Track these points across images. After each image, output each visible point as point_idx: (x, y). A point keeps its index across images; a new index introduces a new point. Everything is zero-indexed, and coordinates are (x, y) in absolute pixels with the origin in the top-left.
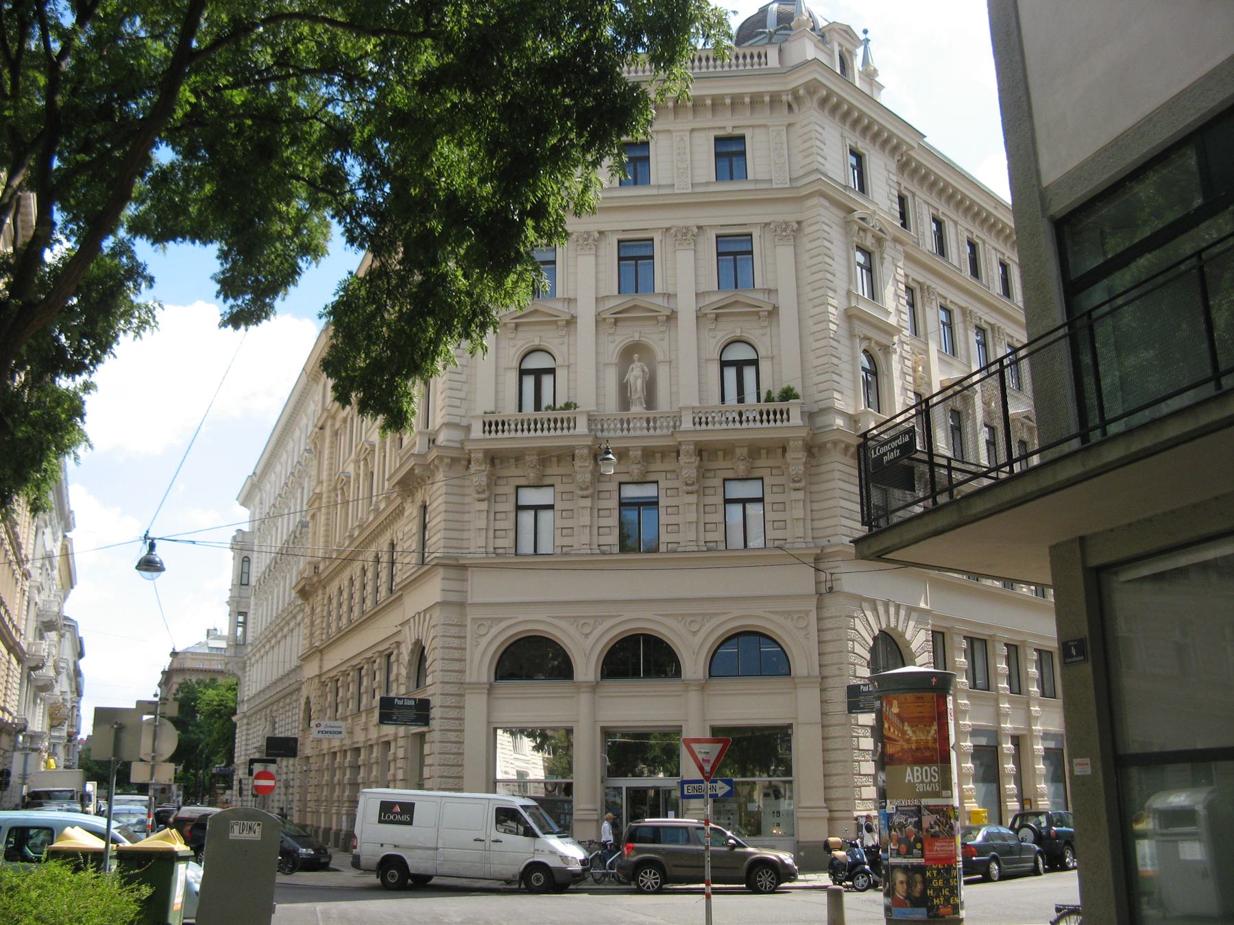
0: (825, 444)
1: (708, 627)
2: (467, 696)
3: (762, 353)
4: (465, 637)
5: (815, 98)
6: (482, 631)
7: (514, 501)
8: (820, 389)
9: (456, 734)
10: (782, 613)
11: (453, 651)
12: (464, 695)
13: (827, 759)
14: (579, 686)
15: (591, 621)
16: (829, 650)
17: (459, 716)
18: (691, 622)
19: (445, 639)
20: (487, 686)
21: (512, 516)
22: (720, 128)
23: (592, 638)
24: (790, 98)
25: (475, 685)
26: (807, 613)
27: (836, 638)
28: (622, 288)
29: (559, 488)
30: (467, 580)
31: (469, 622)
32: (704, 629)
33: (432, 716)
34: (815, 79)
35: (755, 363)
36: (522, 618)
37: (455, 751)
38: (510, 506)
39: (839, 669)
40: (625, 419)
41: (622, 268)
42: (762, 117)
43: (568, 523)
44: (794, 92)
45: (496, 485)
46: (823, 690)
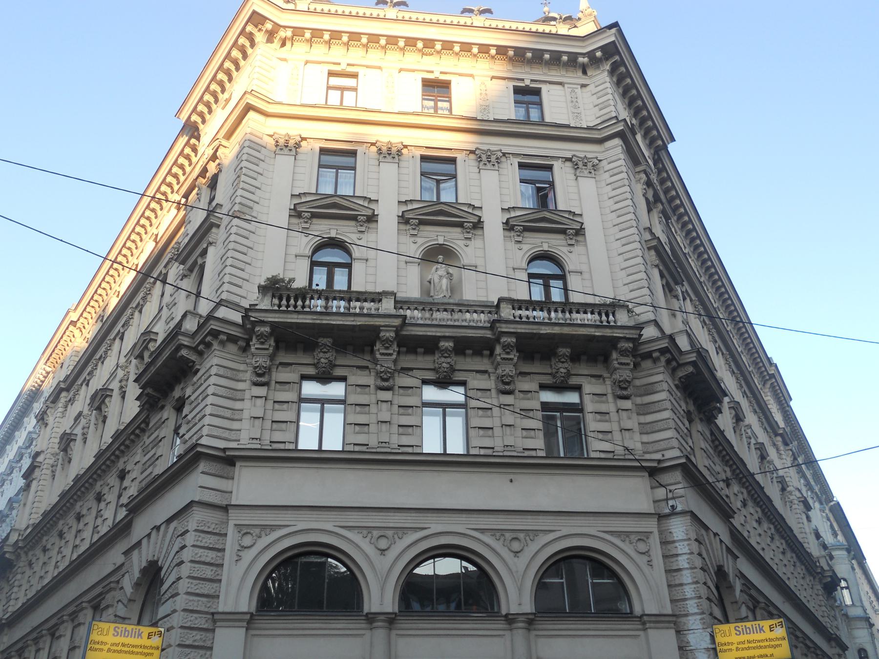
0: (651, 353)
1: (534, 547)
3: (570, 266)
4: (223, 550)
6: (247, 541)
10: (492, 531)
12: (213, 631)
19: (197, 550)
20: (248, 617)
22: (334, 64)
23: (392, 554)
25: (231, 618)
31: (231, 531)
36: (565, 531)
43: (362, 419)
46: (678, 632)
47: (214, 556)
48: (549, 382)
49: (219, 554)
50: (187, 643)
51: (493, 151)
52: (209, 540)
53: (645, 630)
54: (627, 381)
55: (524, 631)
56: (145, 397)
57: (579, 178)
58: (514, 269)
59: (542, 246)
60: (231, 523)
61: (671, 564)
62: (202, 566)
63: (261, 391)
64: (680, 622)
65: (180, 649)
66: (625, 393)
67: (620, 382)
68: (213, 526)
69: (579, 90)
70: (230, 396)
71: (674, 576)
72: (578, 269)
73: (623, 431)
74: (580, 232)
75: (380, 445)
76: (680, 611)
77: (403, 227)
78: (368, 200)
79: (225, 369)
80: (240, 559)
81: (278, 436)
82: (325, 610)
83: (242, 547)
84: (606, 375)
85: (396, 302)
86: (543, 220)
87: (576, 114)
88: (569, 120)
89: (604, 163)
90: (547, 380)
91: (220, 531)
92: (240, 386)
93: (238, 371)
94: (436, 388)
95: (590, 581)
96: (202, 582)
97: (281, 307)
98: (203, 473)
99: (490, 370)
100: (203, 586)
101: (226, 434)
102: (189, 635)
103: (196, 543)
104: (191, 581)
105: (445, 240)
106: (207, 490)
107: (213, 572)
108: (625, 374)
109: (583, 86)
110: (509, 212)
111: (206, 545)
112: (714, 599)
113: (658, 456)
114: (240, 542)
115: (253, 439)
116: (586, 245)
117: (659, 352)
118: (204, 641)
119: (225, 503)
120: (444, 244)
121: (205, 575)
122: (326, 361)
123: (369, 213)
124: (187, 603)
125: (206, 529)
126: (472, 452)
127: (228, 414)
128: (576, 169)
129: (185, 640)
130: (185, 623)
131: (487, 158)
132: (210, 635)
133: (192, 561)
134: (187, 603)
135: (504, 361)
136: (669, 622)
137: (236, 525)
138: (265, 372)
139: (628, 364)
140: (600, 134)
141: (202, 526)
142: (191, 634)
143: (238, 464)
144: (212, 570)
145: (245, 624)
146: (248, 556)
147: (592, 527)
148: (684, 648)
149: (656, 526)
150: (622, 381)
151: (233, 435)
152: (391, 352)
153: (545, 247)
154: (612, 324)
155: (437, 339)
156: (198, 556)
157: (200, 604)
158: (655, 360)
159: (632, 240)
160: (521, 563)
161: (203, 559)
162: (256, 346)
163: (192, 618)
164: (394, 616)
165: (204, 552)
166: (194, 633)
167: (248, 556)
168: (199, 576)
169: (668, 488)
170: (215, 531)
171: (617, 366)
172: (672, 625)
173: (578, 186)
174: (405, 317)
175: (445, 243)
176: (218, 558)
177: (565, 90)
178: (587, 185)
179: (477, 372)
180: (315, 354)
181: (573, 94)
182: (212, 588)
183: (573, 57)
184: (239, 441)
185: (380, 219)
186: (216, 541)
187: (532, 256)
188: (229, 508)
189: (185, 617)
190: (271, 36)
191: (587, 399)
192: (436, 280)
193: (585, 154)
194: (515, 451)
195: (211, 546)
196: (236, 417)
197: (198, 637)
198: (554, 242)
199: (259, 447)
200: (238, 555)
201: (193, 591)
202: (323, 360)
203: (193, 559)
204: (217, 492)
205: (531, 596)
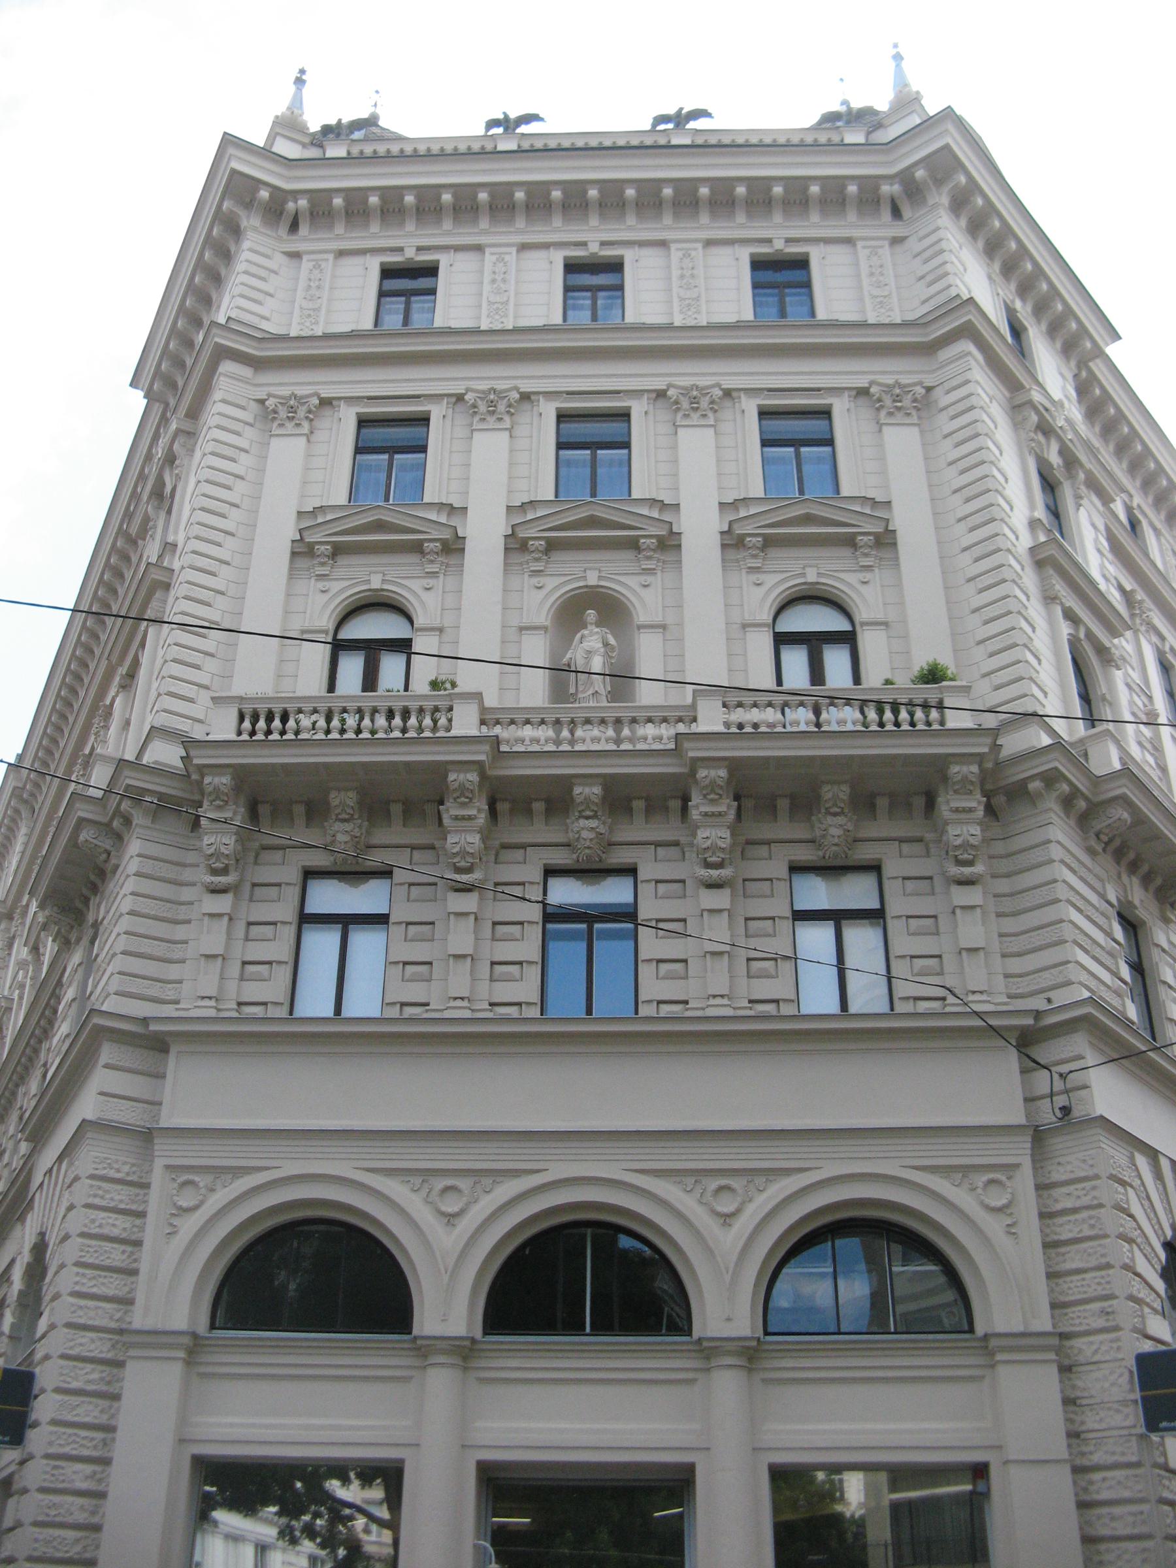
0: (1024, 783)
2: (130, 1365)
3: (862, 614)
5: (946, 189)
7: (296, 901)
8: (999, 682)
9: (88, 1469)
11: (108, 1246)
12: (120, 1364)
13: (1092, 1532)
14: (425, 1350)
15: (464, 1184)
16: (1069, 1266)
17: (103, 1419)
18: (721, 1189)
19: (94, 1214)
21: (289, 932)
24: (896, 188)
26: (1011, 1168)
27: (1087, 1232)
28: (561, 489)
29: (400, 876)
30: (163, 1076)
31: (157, 1177)
32: (750, 1208)
33: (33, 1416)
34: (1056, 768)
35: (848, 639)
37: (81, 1517)
38: (286, 911)
39: (1105, 1313)
40: (565, 718)
41: (563, 471)
42: (849, 224)
44: (906, 178)
45: (256, 863)
46: (1066, 1370)
47: (128, 1225)
48: (810, 858)
49: (138, 1222)
50: (75, 1385)
51: (302, 397)
53: (993, 1366)
54: (973, 846)
56: (53, 926)
57: (885, 428)
59: (803, 575)
60: (159, 1164)
61: (1058, 1230)
62: (103, 1244)
63: (223, 903)
64: (1071, 1347)
65: (58, 1397)
66: (967, 870)
68: (126, 1168)
70: (165, 915)
71: (1063, 1254)
73: (964, 954)
74: (886, 541)
75: (453, 1004)
76: (1072, 1325)
77: (732, 554)
78: (448, 509)
79: (156, 863)
80: (175, 1233)
81: (253, 991)
82: (664, 1331)
83: (180, 1208)
84: (929, 836)
85: (483, 710)
86: (808, 519)
89: (938, 392)
90: (804, 855)
91: (141, 1177)
92: (187, 894)
93: (184, 865)
94: (579, 883)
96: (103, 1274)
97: (423, 732)
98: (106, 1066)
99: (683, 840)
100: (105, 1281)
101: (154, 990)
102: (78, 1372)
103: (90, 1200)
104: (81, 1270)
105: (600, 578)
106: (116, 1100)
107: (127, 1254)
110: (737, 509)
111: (112, 1204)
112: (1150, 1298)
113: (1039, 1004)
114: (175, 1198)
115: (203, 998)
117: (1042, 781)
118: (109, 1383)
120: (818, 583)
121: (110, 1261)
122: (592, 835)
123: (446, 535)
124: (74, 1312)
125: (112, 1174)
126: (900, 1008)
127: (159, 949)
128: (878, 409)
129: (69, 1379)
130: (71, 1348)
131: (894, 401)
133: (83, 1235)
134: (74, 1312)
135: (460, 823)
137: (167, 1167)
138: (227, 865)
139: (970, 810)
141: (105, 1168)
142: (82, 1369)
144: (124, 1252)
145: (181, 1354)
146: (189, 1225)
148: (1078, 1402)
149: (1029, 1152)
150: (457, 854)
151: (169, 993)
152: (473, 812)
153: (811, 576)
154: (936, 726)
155: (566, 783)
156: (97, 1224)
157: (103, 1314)
161: (105, 1231)
162: (703, 809)
163: (83, 1340)
164: (754, 1343)
165: (110, 1218)
166: (89, 1367)
167: (189, 1225)
168: (97, 1262)
169: (1053, 1069)
170: (129, 1178)
172: (1052, 1356)
174: (497, 740)
175: (385, 587)
176: (135, 1229)
180: (568, 821)
182: (125, 1285)
184: (177, 1002)
185: (685, 542)
186: (133, 1197)
187: (784, 595)
188: (155, 1134)
189: (70, 1337)
193: (896, 377)
194: (989, 1002)
195: (122, 1206)
196: (176, 956)
197: (95, 1376)
199: (467, 1014)
200: (171, 1225)
201: (84, 1289)
202: (341, 838)
203: (86, 1230)
204: (135, 1104)
205: (753, 1301)
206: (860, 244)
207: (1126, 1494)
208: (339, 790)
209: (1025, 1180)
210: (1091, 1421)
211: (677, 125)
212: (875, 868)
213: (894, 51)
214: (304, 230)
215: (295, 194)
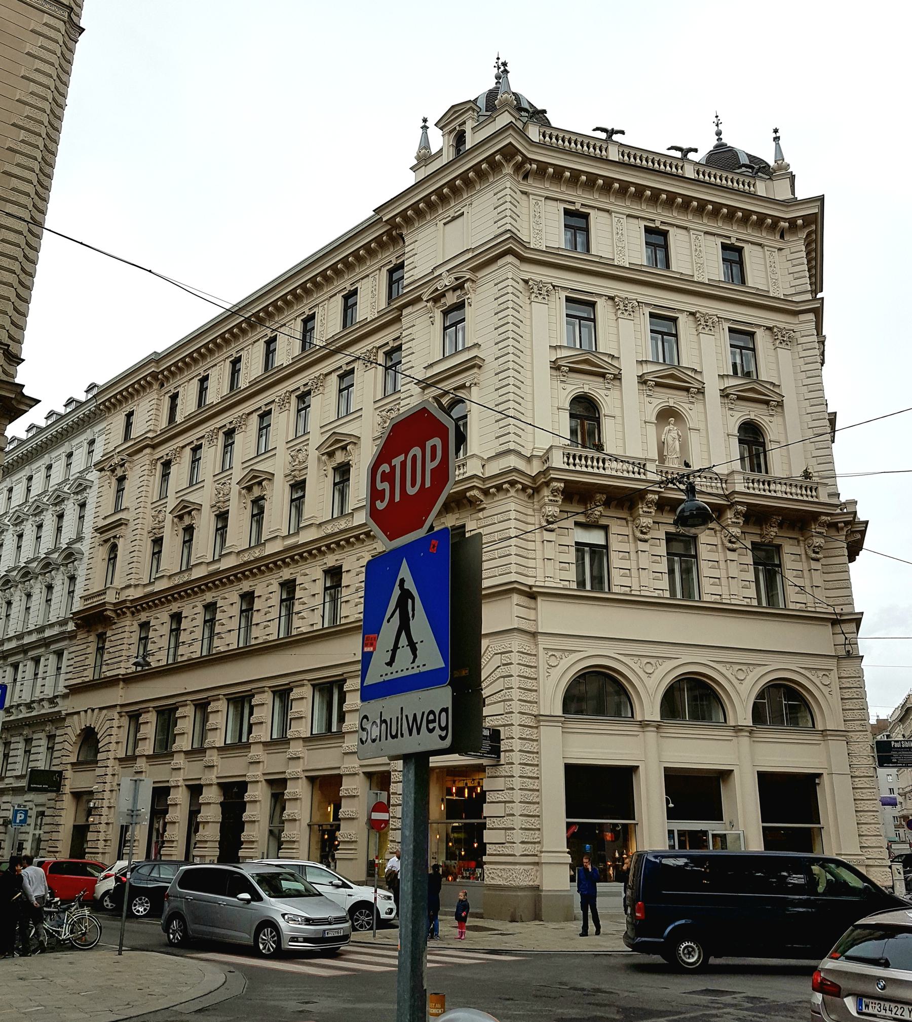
31: (541, 652)
52: (526, 660)
55: (748, 738)
58: (558, 409)
60: (541, 647)
67: (548, 516)
69: (776, 254)
72: (697, 427)
84: (629, 518)
87: (620, 248)
88: (613, 253)
89: (798, 335)
90: (581, 519)
95: (784, 702)
105: (674, 403)
108: (818, 541)
109: (780, 249)
110: (556, 349)
116: (621, 390)
119: (533, 630)
122: (599, 513)
132: (535, 731)
136: (558, 721)
140: (797, 307)
143: (539, 599)
147: (609, 650)
158: (838, 530)
159: (821, 417)
160: (651, 683)
171: (814, 534)
172: (655, 729)
173: (618, 327)
177: (764, 252)
178: (784, 355)
179: (789, 538)
181: (537, 207)
183: (776, 220)
190: (518, 167)
191: (613, 539)
192: (670, 442)
198: (678, 399)
206: (766, 248)
207: (868, 786)
208: (600, 493)
209: (834, 675)
210: (855, 761)
211: (610, 137)
212: (605, 528)
213: (774, 135)
214: (530, 181)
215: (531, 161)
